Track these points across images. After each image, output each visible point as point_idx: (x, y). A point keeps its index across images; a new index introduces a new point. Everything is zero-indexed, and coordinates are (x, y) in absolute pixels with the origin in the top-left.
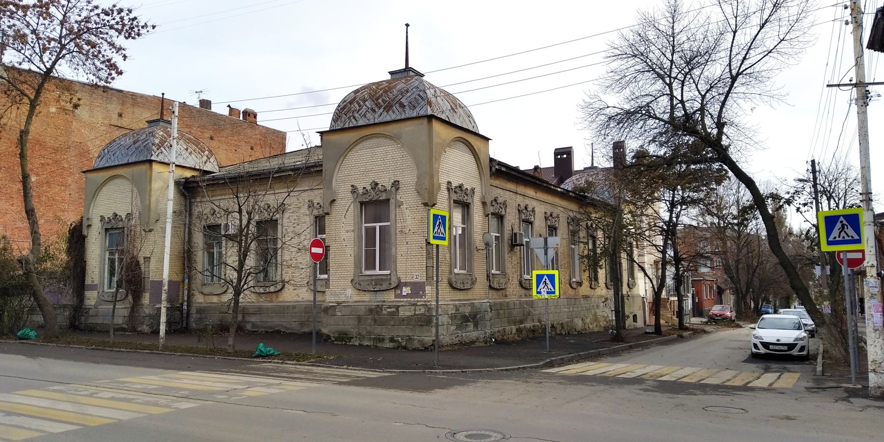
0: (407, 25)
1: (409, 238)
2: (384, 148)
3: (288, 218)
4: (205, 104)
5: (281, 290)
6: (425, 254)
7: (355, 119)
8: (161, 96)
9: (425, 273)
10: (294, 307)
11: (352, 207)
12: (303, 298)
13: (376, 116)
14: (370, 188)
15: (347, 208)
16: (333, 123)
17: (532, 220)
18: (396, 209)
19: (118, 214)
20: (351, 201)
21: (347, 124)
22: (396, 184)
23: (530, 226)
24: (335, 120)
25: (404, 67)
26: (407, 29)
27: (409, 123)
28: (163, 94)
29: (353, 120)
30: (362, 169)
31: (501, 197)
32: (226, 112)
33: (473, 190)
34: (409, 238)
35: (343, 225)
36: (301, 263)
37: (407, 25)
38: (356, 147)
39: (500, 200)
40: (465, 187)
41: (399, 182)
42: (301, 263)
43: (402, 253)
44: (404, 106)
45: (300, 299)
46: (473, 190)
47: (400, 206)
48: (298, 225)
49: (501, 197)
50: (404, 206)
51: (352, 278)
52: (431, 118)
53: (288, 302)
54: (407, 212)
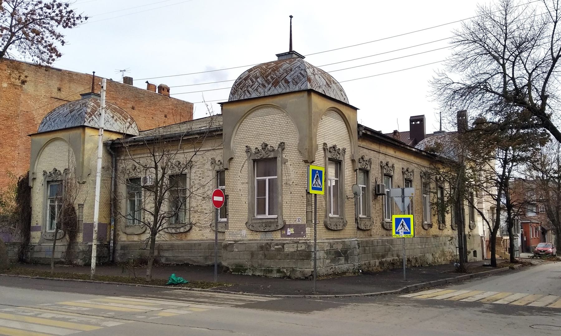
0: (291, 17)
2: (272, 116)
3: (195, 173)
4: (128, 80)
7: (249, 93)
8: (92, 74)
9: (306, 217)
12: (207, 237)
13: (266, 90)
14: (261, 148)
15: (242, 164)
16: (231, 96)
18: (282, 165)
20: (245, 159)
21: (243, 96)
22: (282, 145)
23: (390, 179)
26: (291, 20)
28: (94, 72)
29: (247, 94)
32: (144, 87)
33: (344, 150)
35: (239, 178)
36: (205, 209)
37: (291, 17)
38: (250, 115)
39: (366, 158)
41: (284, 143)
44: (288, 82)
45: (204, 238)
46: (344, 150)
47: (285, 163)
48: (203, 178)
50: (289, 163)
51: (247, 221)
54: (291, 168)
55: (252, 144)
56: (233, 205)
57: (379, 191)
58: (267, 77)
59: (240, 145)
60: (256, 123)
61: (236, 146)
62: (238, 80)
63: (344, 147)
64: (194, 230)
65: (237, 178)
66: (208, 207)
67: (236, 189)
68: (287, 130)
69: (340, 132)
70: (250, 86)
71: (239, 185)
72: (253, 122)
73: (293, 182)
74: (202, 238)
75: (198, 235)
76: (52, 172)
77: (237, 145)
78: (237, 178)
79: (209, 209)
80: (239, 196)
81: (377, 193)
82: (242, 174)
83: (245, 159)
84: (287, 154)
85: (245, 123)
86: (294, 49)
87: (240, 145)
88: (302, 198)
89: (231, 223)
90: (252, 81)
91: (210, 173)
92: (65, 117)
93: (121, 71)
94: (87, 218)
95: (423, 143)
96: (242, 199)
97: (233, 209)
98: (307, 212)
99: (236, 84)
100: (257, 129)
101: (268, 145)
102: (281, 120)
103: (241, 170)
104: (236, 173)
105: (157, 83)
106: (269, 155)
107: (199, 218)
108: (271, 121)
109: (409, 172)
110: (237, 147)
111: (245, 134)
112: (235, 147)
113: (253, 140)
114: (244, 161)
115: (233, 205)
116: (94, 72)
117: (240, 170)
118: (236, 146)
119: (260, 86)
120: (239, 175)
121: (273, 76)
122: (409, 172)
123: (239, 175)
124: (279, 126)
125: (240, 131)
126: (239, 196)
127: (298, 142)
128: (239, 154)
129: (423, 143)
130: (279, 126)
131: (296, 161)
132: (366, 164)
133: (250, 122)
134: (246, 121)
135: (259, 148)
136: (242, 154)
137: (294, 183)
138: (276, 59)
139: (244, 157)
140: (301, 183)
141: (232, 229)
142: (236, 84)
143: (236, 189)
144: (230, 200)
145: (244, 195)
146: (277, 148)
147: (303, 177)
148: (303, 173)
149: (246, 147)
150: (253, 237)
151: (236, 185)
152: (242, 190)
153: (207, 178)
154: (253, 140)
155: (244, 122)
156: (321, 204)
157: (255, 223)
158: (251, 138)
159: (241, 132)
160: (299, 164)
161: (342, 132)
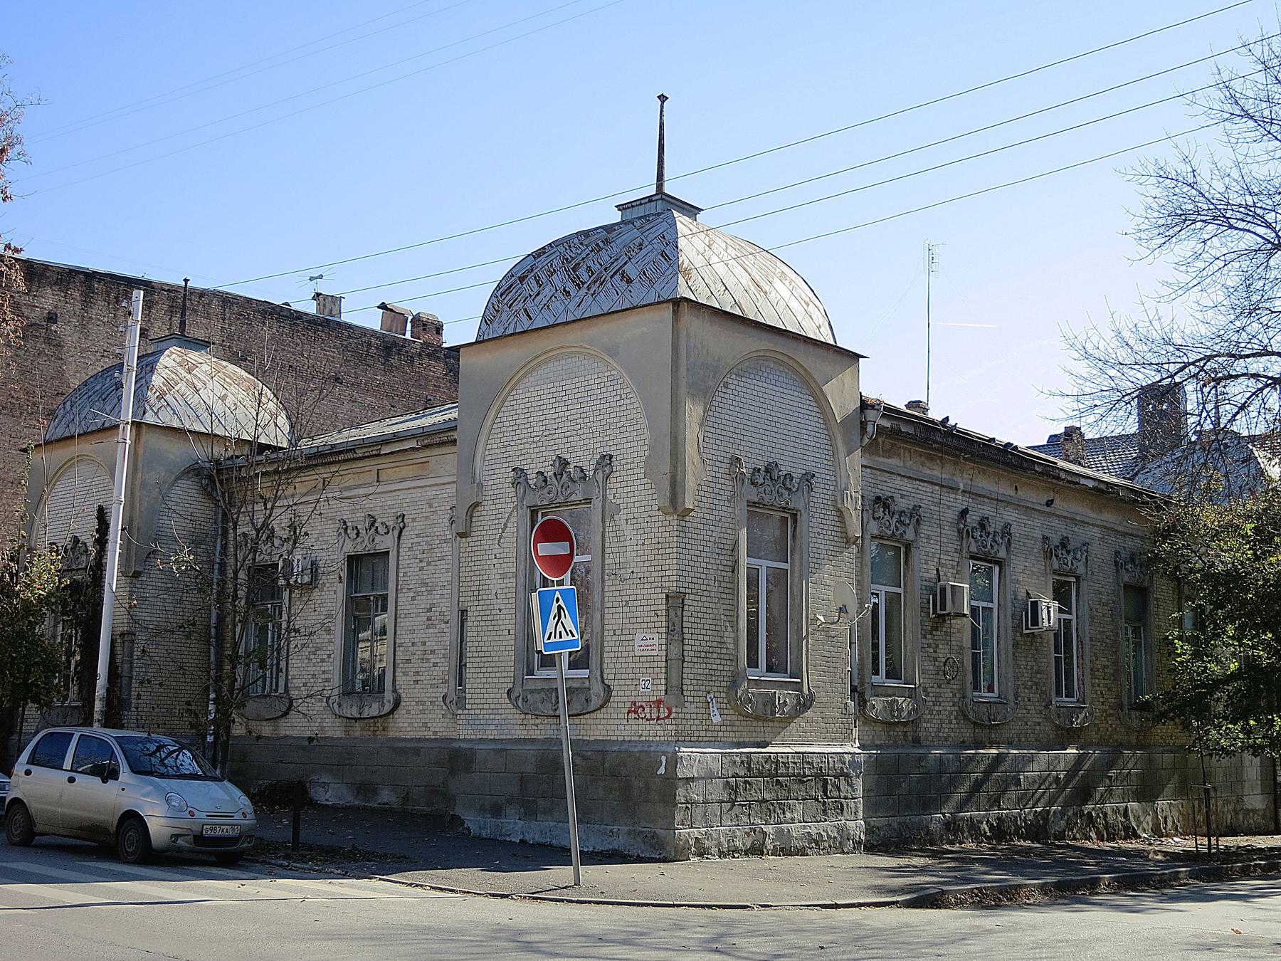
0: (663, 98)
1: (630, 592)
2: (582, 379)
3: (410, 549)
4: (328, 302)
5: (392, 712)
6: (664, 630)
7: (528, 315)
8: (184, 283)
9: (663, 676)
10: (417, 751)
11: (514, 519)
12: (435, 733)
13: (572, 307)
14: (550, 474)
15: (503, 521)
16: (484, 327)
17: (1002, 554)
18: (603, 522)
19: (82, 539)
20: (511, 505)
21: (512, 325)
22: (606, 461)
23: (997, 569)
24: (486, 320)
25: (652, 191)
26: (662, 107)
27: (633, 318)
28: (186, 281)
29: (524, 318)
30: (537, 429)
31: (903, 496)
32: (373, 321)
33: (808, 478)
34: (630, 592)
35: (495, 561)
36: (433, 652)
37: (663, 98)
38: (526, 380)
39: (902, 504)
40: (575, 459)
41: (611, 457)
42: (433, 652)
43: (616, 627)
44: (629, 281)
45: (430, 735)
46: (808, 478)
47: (612, 516)
48: (429, 563)
49: (903, 496)
50: (623, 516)
51: (511, 685)
52: (678, 303)
53: (405, 740)
54: (628, 531)
55: (529, 461)
56: (479, 639)
57: (943, 607)
58: (574, 269)
59: (498, 466)
60: (541, 403)
61: (490, 467)
62: (504, 282)
63: (811, 469)
64: (404, 712)
65: (489, 562)
66: (441, 647)
67: (488, 592)
68: (618, 420)
69: (795, 424)
70: (531, 296)
71: (494, 581)
72: (532, 399)
73: (632, 572)
74: (426, 733)
75: (415, 725)
76: (69, 547)
77: (494, 467)
78: (489, 562)
79: (443, 651)
80: (493, 612)
81: (939, 612)
82: (501, 551)
83: (510, 505)
84: (620, 490)
85: (514, 403)
86: (667, 190)
87: (498, 466)
88: (655, 619)
89: (472, 691)
90: (537, 282)
91: (446, 549)
92: (104, 400)
93: (311, 279)
94: (144, 670)
95: (1159, 466)
96: (500, 622)
97: (479, 649)
98: (666, 661)
99: (499, 292)
100: (542, 418)
101: (568, 463)
102: (604, 390)
103: (501, 537)
104: (487, 547)
105: (411, 307)
106: (571, 494)
107: (418, 678)
108: (579, 395)
109: (1068, 552)
110: (492, 472)
111: (513, 433)
112: (486, 473)
113: (531, 451)
114: (509, 510)
115: (479, 639)
116: (186, 281)
117: (498, 537)
118: (490, 467)
119: (559, 294)
120: (494, 552)
121: (592, 265)
122: (1068, 552)
123: (494, 552)
124: (599, 407)
125: (500, 425)
126: (493, 612)
127: (647, 453)
128: (496, 492)
129: (1159, 466)
130: (599, 407)
131: (642, 509)
132: (902, 522)
133: (527, 400)
134: (517, 397)
135: (545, 474)
136: (503, 491)
137: (635, 575)
138: (616, 217)
139: (508, 500)
140: (654, 574)
141: (474, 707)
142: (499, 292)
143: (488, 592)
144: (471, 624)
145: (505, 612)
146: (592, 472)
147: (660, 557)
148: (660, 546)
149: (513, 470)
150: (526, 732)
151: (488, 582)
152: (503, 596)
153: (439, 563)
154: (531, 451)
155: (510, 398)
156: (718, 639)
157: (532, 691)
158: (528, 446)
159: (503, 430)
160: (649, 519)
161: (801, 426)
